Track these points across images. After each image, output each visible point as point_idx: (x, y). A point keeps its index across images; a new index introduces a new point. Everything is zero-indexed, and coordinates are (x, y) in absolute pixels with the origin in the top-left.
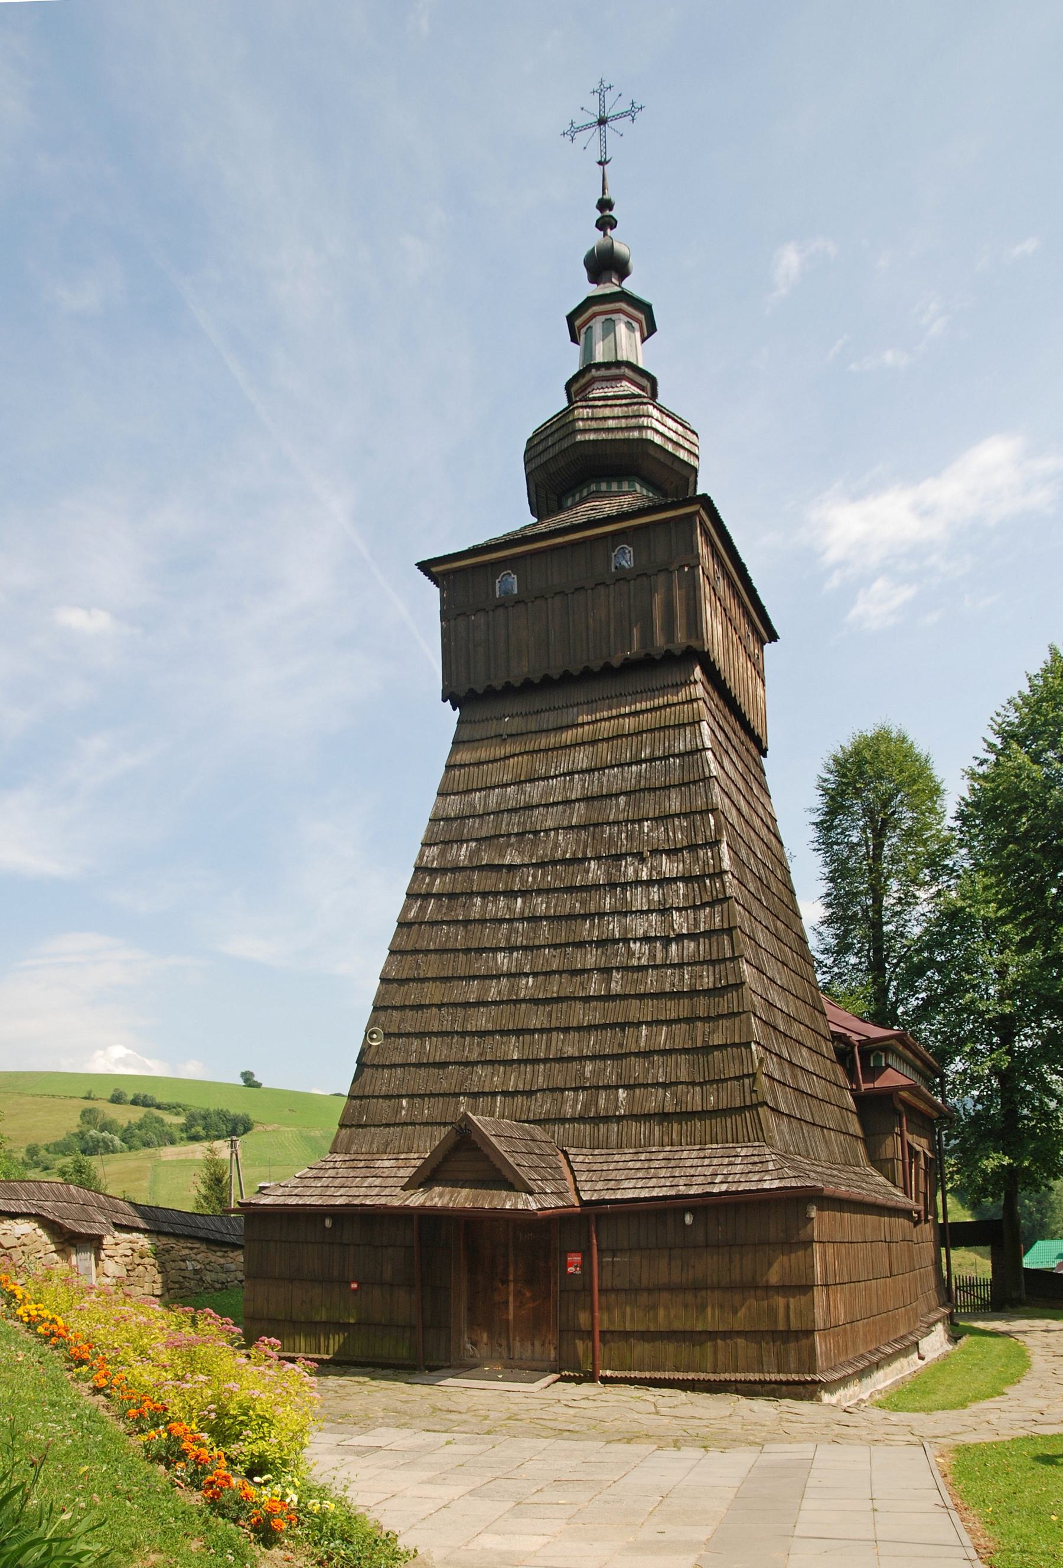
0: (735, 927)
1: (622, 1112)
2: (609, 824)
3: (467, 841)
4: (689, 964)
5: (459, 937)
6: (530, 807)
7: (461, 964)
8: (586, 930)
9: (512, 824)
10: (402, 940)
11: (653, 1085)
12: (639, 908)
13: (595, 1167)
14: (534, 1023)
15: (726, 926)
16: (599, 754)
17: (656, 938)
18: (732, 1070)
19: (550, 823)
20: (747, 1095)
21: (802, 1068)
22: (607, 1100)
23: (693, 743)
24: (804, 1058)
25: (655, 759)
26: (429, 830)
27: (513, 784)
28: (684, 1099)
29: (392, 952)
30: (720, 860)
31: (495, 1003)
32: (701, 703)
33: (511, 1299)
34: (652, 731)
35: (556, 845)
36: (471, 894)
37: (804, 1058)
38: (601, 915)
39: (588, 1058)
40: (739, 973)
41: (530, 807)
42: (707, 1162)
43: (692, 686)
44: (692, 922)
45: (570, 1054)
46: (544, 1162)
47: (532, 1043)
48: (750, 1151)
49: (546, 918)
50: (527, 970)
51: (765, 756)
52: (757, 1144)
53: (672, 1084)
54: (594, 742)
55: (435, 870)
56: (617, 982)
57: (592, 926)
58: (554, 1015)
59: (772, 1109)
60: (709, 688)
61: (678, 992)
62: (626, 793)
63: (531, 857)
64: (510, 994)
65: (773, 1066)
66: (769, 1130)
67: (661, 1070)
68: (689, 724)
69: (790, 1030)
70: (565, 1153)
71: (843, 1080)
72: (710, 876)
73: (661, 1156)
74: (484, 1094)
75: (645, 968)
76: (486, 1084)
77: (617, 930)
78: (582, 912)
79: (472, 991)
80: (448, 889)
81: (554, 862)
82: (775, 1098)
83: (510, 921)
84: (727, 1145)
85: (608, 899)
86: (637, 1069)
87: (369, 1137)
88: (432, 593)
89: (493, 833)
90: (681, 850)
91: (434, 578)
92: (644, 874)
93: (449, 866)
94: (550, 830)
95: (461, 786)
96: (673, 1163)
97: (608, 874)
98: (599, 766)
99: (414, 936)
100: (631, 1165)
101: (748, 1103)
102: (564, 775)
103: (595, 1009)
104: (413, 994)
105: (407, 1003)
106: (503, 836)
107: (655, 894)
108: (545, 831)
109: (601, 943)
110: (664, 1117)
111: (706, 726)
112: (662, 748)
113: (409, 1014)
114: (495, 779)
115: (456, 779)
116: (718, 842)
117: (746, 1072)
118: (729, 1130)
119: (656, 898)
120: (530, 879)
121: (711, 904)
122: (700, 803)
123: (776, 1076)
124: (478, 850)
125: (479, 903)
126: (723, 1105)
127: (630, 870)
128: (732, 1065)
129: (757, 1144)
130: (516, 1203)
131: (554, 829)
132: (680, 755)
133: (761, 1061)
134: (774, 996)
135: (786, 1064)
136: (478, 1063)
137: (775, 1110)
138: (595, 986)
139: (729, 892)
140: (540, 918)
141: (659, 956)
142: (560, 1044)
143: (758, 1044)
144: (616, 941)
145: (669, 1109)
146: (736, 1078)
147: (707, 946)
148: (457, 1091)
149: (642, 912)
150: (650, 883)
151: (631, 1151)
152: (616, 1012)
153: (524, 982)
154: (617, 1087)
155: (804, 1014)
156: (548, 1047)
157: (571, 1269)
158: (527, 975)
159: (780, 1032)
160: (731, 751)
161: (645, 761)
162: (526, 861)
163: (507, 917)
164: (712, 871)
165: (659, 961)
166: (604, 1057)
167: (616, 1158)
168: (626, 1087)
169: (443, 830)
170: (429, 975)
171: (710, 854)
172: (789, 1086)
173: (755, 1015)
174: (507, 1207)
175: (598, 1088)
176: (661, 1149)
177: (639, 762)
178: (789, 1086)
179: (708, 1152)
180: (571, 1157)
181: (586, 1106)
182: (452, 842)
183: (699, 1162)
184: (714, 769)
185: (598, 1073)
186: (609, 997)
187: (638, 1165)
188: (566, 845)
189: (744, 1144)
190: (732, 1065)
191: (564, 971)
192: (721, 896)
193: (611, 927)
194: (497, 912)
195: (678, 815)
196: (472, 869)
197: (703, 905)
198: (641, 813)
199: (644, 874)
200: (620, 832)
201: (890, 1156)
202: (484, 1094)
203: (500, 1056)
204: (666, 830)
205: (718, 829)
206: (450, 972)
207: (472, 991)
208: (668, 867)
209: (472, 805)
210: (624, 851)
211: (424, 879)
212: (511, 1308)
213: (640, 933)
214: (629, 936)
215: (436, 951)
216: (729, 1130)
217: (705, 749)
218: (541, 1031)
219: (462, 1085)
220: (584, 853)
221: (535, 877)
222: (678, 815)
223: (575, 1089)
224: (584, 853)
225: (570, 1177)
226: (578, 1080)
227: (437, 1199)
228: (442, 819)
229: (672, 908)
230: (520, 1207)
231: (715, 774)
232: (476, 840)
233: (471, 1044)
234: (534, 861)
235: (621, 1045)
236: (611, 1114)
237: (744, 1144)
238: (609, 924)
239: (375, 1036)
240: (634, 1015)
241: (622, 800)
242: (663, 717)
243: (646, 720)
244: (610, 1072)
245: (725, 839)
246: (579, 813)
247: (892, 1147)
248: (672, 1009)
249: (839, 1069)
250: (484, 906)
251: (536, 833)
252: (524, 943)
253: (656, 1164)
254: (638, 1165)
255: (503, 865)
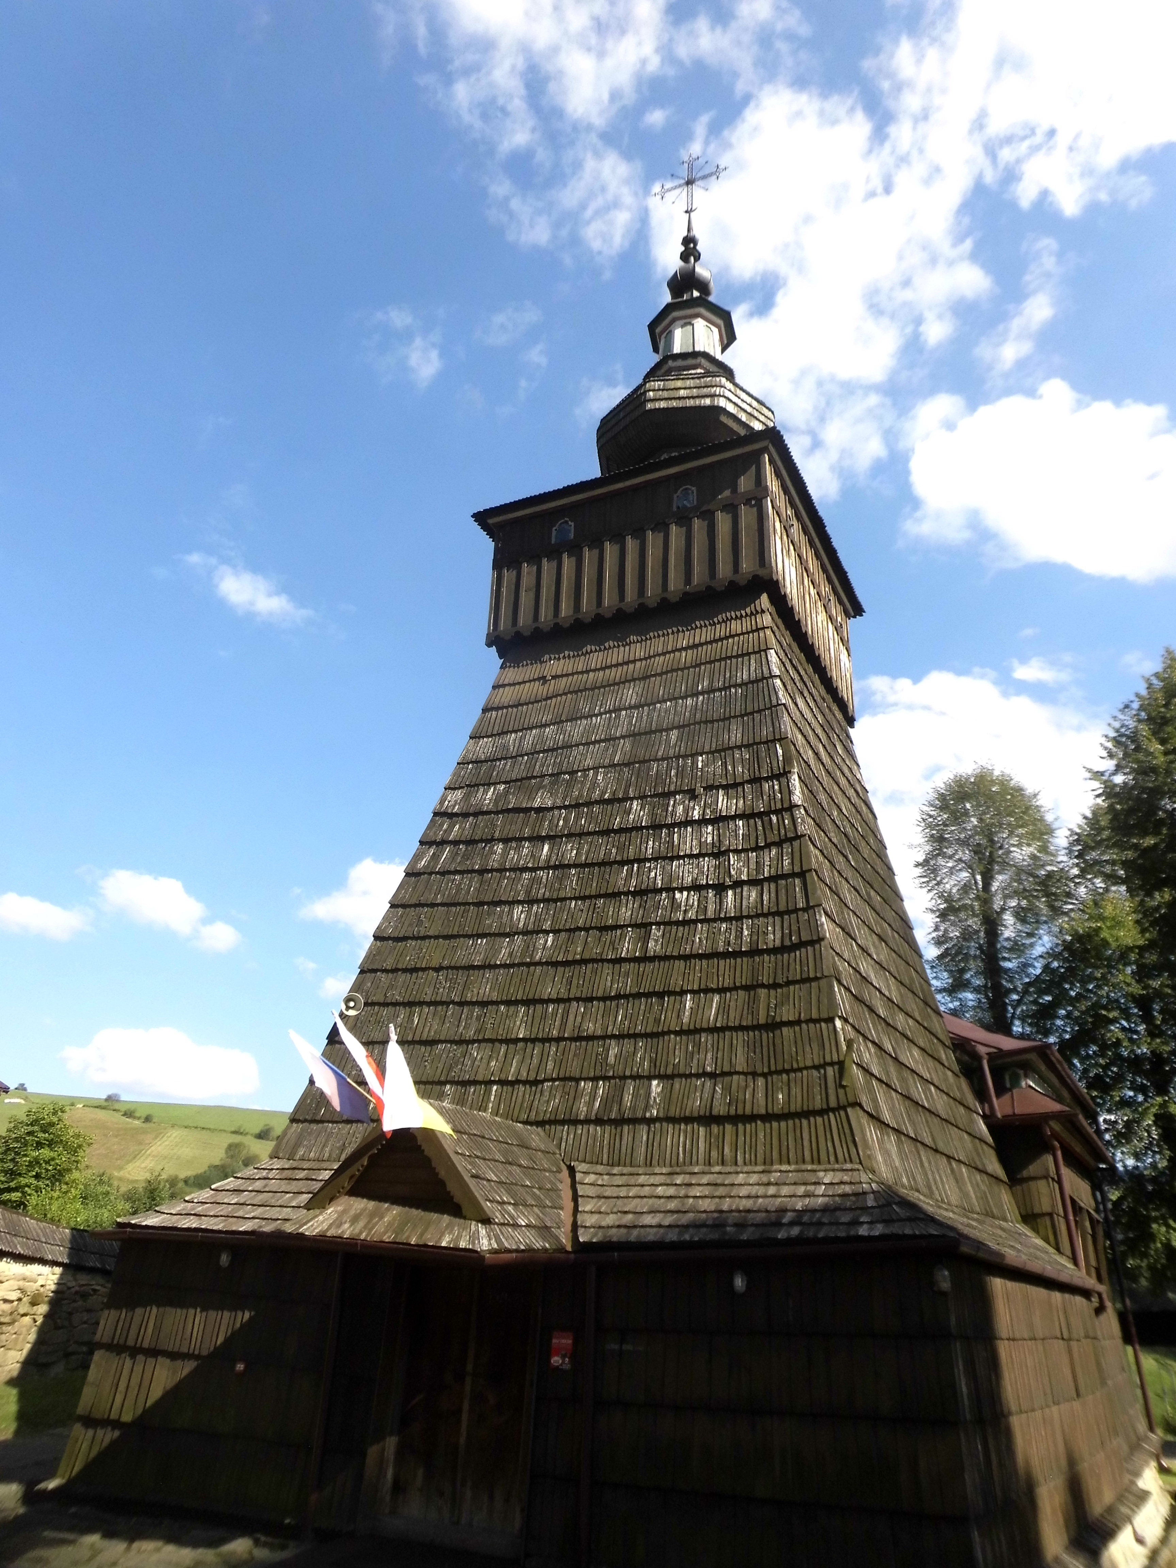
0: (810, 870)
1: (655, 1112)
2: (656, 760)
3: (495, 784)
4: (748, 917)
5: (470, 888)
6: (568, 746)
7: (469, 920)
8: (622, 878)
9: (547, 764)
10: (406, 893)
11: (698, 1076)
12: (688, 852)
13: (609, 1192)
14: (548, 991)
15: (797, 869)
16: (651, 689)
17: (708, 886)
18: (809, 1056)
19: (589, 762)
20: (831, 1091)
21: (912, 1070)
22: (636, 1095)
23: (759, 671)
24: (912, 1057)
25: (714, 691)
26: (456, 774)
27: (554, 724)
28: (741, 1097)
29: (393, 906)
30: (790, 793)
31: (504, 966)
32: (768, 632)
33: (466, 1406)
34: (711, 662)
35: (594, 784)
36: (491, 840)
37: (912, 1057)
38: (641, 861)
39: (613, 1036)
40: (816, 926)
41: (568, 746)
42: (772, 1190)
43: (758, 616)
44: (753, 866)
45: (590, 1032)
46: (531, 1178)
47: (544, 1017)
48: (838, 1177)
49: (575, 866)
50: (547, 926)
51: (852, 726)
52: (848, 1166)
53: (724, 1074)
54: (645, 678)
55: (456, 815)
56: (656, 941)
57: (630, 873)
58: (575, 981)
59: (871, 1115)
60: (776, 617)
61: (734, 952)
62: (678, 727)
63: (564, 799)
64: (523, 955)
65: (867, 1054)
66: (866, 1146)
67: (709, 1055)
68: (755, 653)
69: (893, 1019)
70: (572, 1171)
71: (970, 1099)
72: (777, 812)
73: (705, 1179)
74: (475, 1083)
75: (695, 922)
76: (480, 1070)
77: (659, 878)
78: (619, 858)
79: (478, 950)
80: (467, 835)
81: (589, 804)
82: (875, 1100)
83: (533, 870)
84: (804, 1167)
85: (651, 843)
86: (677, 1053)
87: (322, 1139)
88: (486, 546)
89: (524, 775)
90: (742, 784)
91: (485, 526)
92: (696, 813)
93: (472, 810)
94: (589, 770)
95: (496, 728)
96: (721, 1191)
97: (652, 814)
98: (649, 701)
99: (421, 887)
100: (660, 1190)
101: (833, 1103)
102: (610, 712)
103: (627, 974)
104: (411, 953)
105: (400, 966)
106: (535, 777)
107: (709, 833)
108: (584, 770)
109: (639, 893)
110: (708, 1119)
111: (774, 655)
112: (722, 679)
113: (402, 977)
114: (534, 720)
115: (492, 721)
116: (786, 774)
117: (828, 1059)
118: (806, 1143)
119: (710, 839)
120: (561, 823)
121: (779, 844)
122: (765, 732)
123: (875, 1071)
124: (506, 792)
125: (500, 851)
126: (796, 1106)
127: (678, 809)
128: (808, 1049)
129: (848, 1166)
130: (459, 1237)
131: (593, 769)
132: (743, 684)
133: (850, 1043)
134: (865, 967)
135: (890, 1062)
136: (474, 1041)
137: (875, 1118)
138: (627, 947)
139: (801, 829)
140: (569, 866)
141: (711, 908)
142: (579, 1019)
143: (846, 1020)
144: (660, 891)
145: (720, 1109)
146: (816, 1067)
147: (773, 895)
148: (442, 1079)
149: (691, 856)
150: (703, 822)
151: (664, 1171)
152: (653, 977)
153: (542, 942)
154: (650, 1078)
155: (913, 1005)
156: (564, 1023)
157: (556, 1360)
158: (547, 932)
159: (879, 1016)
160: (806, 694)
161: (702, 693)
162: (559, 803)
163: (530, 865)
164: (779, 806)
165: (710, 914)
166: (635, 1036)
167: (642, 1179)
168: (660, 1077)
169: (472, 774)
170: (430, 933)
171: (776, 787)
172: (896, 1091)
173: (839, 982)
174: (444, 1244)
175: (624, 1078)
176: (706, 1169)
177: (697, 694)
178: (896, 1091)
179: (774, 1177)
180: (578, 1176)
181: (606, 1102)
182: (477, 785)
183: (761, 1190)
184: (783, 697)
185: (625, 1058)
186: (645, 959)
187: (671, 1191)
188: (604, 783)
189: (828, 1167)
190: (808, 1049)
191: (591, 928)
192: (791, 835)
193: (653, 874)
194: (518, 861)
195: (739, 747)
196: (497, 813)
197: (768, 846)
198: (695, 747)
199: (696, 813)
200: (669, 769)
201: (1046, 1208)
202: (475, 1083)
203: (502, 1034)
204: (725, 764)
205: (787, 759)
206: (456, 929)
207: (478, 950)
208: (724, 803)
209: (505, 747)
210: (672, 788)
211: (442, 825)
212: (465, 1417)
213: (688, 881)
214: (675, 885)
215: (442, 904)
216: (806, 1143)
217: (772, 677)
218: (558, 1001)
219: (450, 1069)
220: (626, 792)
221: (566, 820)
222: (739, 747)
223: (595, 1079)
224: (626, 792)
225: (569, 1205)
226: (598, 1067)
227: (347, 1226)
228: (472, 762)
229: (728, 851)
230: (462, 1245)
231: (784, 702)
232: (505, 783)
233: (469, 1017)
234: (567, 803)
235: (657, 1021)
236: (639, 1115)
237: (828, 1167)
238: (650, 871)
239: (352, 1004)
240: (676, 982)
241: (674, 735)
242: (724, 648)
243: (705, 652)
244: (641, 1056)
245: (796, 770)
246: (622, 751)
247: (1044, 1196)
248: (725, 973)
249: (964, 1083)
250: (505, 853)
251: (572, 773)
252: (547, 895)
253: (697, 1191)
254: (671, 1191)
255: (531, 809)
